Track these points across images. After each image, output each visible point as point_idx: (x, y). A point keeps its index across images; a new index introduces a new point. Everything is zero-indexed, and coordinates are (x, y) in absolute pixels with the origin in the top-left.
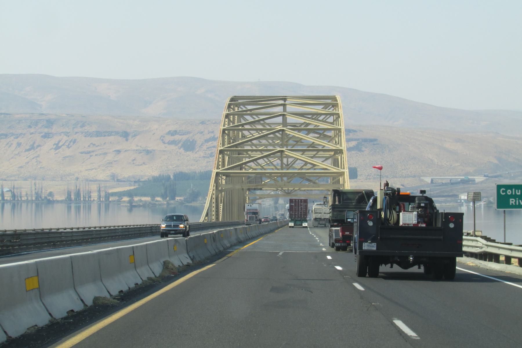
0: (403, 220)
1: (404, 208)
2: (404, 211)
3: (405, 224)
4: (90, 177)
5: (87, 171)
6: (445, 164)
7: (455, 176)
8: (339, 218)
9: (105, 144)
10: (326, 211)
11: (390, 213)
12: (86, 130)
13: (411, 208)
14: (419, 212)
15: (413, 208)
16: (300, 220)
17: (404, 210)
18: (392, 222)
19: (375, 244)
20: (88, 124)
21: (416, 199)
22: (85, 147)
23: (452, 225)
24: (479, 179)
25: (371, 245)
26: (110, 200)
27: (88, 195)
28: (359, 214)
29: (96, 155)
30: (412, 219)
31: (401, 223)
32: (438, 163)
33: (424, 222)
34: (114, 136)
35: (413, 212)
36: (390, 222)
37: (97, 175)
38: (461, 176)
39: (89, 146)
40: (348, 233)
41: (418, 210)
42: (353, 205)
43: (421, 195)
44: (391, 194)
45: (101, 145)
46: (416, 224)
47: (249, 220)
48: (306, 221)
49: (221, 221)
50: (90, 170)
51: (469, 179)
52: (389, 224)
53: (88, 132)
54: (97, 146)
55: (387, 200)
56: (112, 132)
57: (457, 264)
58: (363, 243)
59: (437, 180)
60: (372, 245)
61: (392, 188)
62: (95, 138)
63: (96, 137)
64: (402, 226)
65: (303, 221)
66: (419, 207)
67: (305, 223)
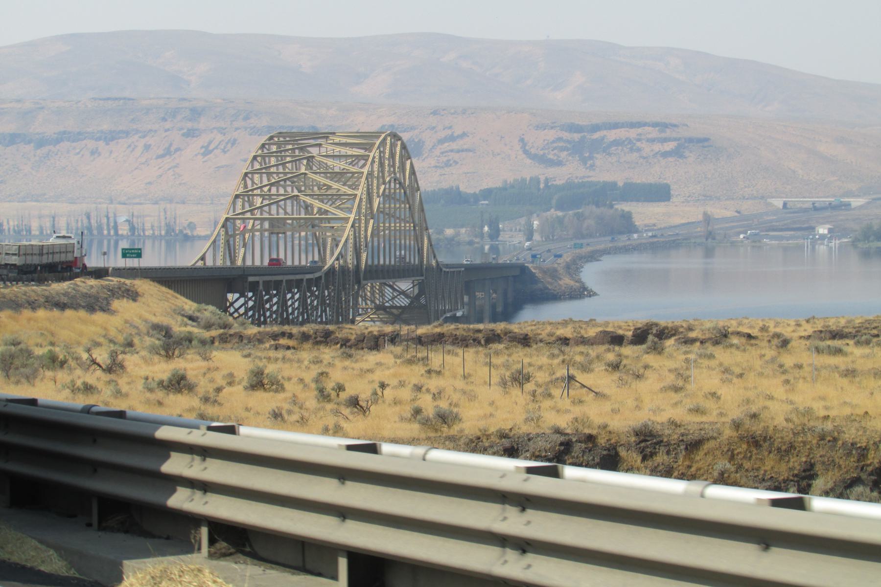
24: (856, 202)
51: (841, 202)
53: (255, 127)
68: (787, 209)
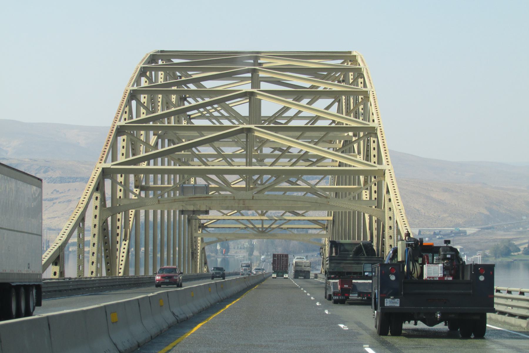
0: (428, 273)
1: (428, 259)
2: (428, 263)
3: (430, 278)
4: (52, 225)
5: (50, 220)
6: (432, 215)
7: (444, 227)
8: (336, 270)
9: (69, 190)
10: (306, 264)
11: (413, 265)
12: (49, 175)
13: (436, 259)
14: (445, 264)
15: (439, 259)
16: (282, 272)
17: (428, 262)
18: (415, 275)
19: (398, 300)
20: (52, 169)
21: (441, 250)
22: (48, 194)
23: (482, 278)
24: (470, 231)
25: (393, 301)
26: (70, 249)
27: (46, 244)
28: (379, 267)
29: (59, 203)
30: (438, 272)
31: (425, 277)
32: (425, 213)
33: (451, 275)
34: (79, 182)
35: (439, 264)
36: (413, 275)
37: (60, 224)
38: (450, 227)
39: (52, 193)
40: (347, 286)
41: (444, 262)
42: (351, 257)
43: (446, 246)
44: (413, 245)
45: (65, 192)
46: (442, 277)
47: (244, 271)
48: (287, 273)
49: (198, 272)
50: (52, 218)
51: (460, 230)
52: (413, 278)
53: (51, 177)
54: (60, 193)
55: (410, 252)
56: (77, 178)
57: (488, 321)
58: (385, 299)
59: (425, 232)
60: (395, 301)
61: (415, 239)
62: (59, 185)
63: (60, 183)
64: (426, 280)
65: (285, 273)
66: (445, 258)
67: (285, 275)
68: (421, 235)
